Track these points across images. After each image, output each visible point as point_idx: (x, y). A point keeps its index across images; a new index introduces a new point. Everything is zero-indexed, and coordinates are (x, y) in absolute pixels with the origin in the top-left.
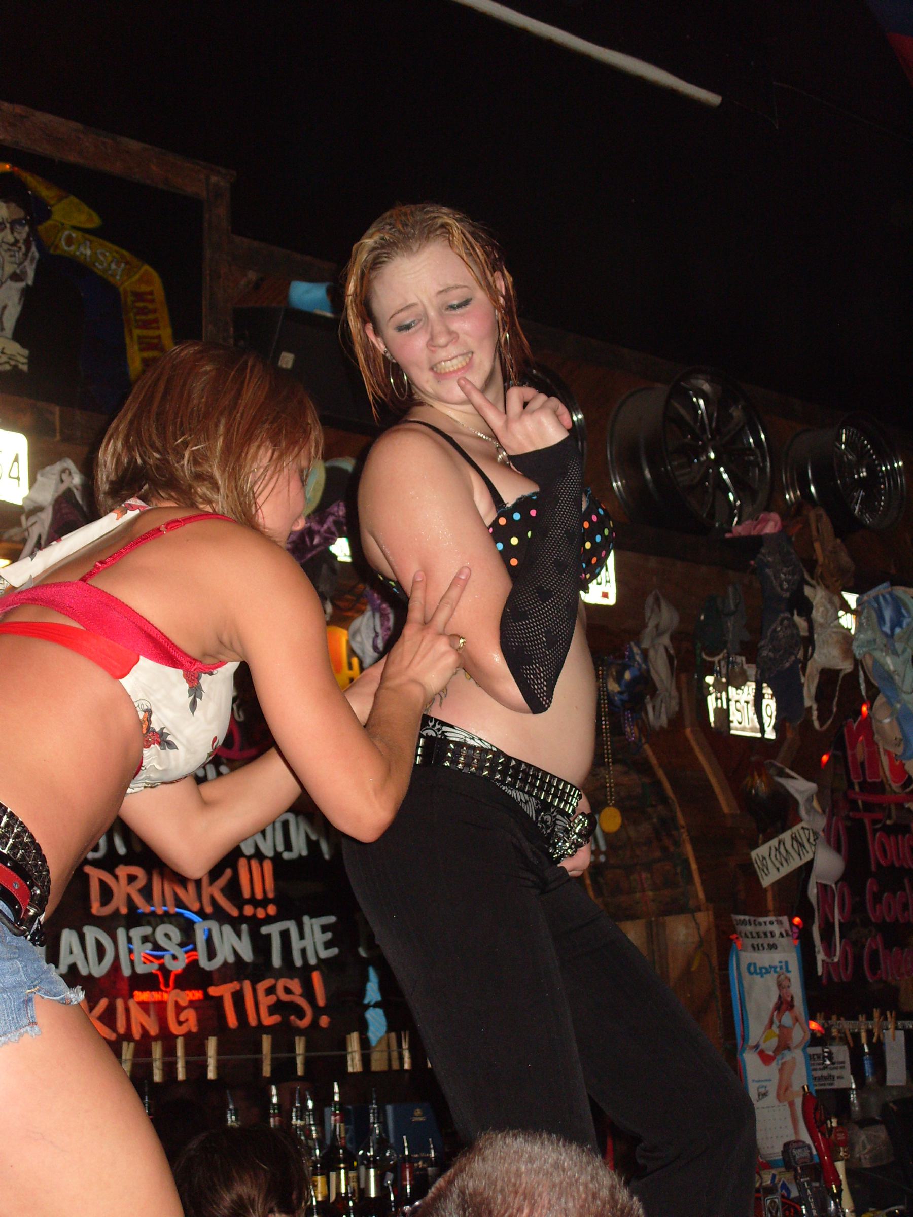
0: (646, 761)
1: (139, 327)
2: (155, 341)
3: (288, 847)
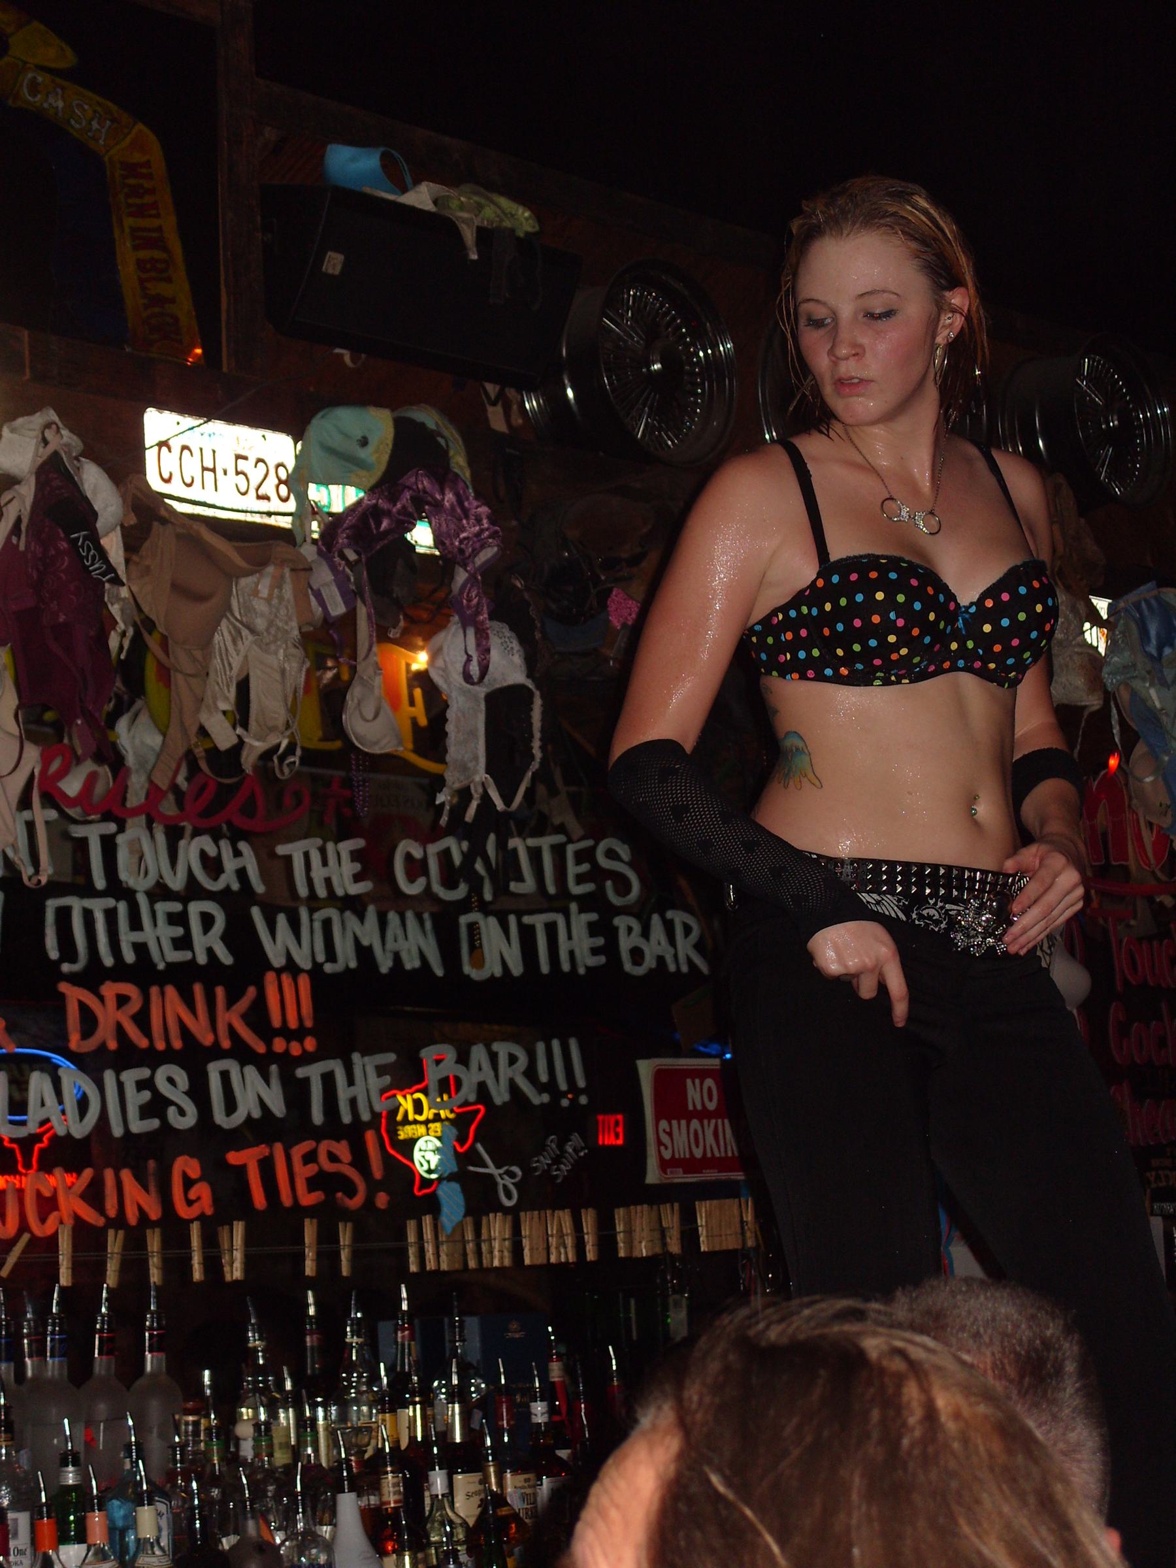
0: (525, 796)
1: (131, 215)
2: (155, 235)
3: (331, 956)
